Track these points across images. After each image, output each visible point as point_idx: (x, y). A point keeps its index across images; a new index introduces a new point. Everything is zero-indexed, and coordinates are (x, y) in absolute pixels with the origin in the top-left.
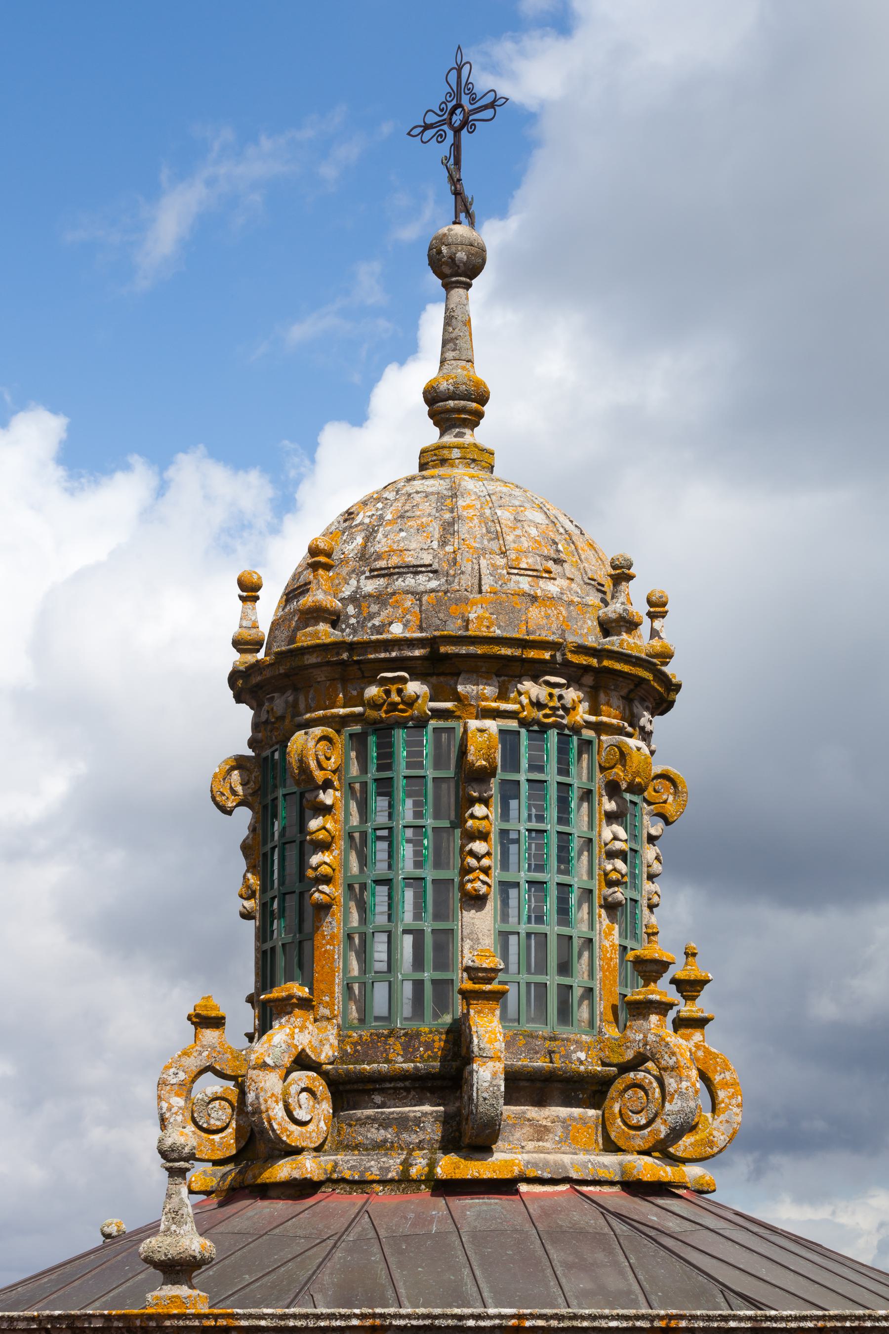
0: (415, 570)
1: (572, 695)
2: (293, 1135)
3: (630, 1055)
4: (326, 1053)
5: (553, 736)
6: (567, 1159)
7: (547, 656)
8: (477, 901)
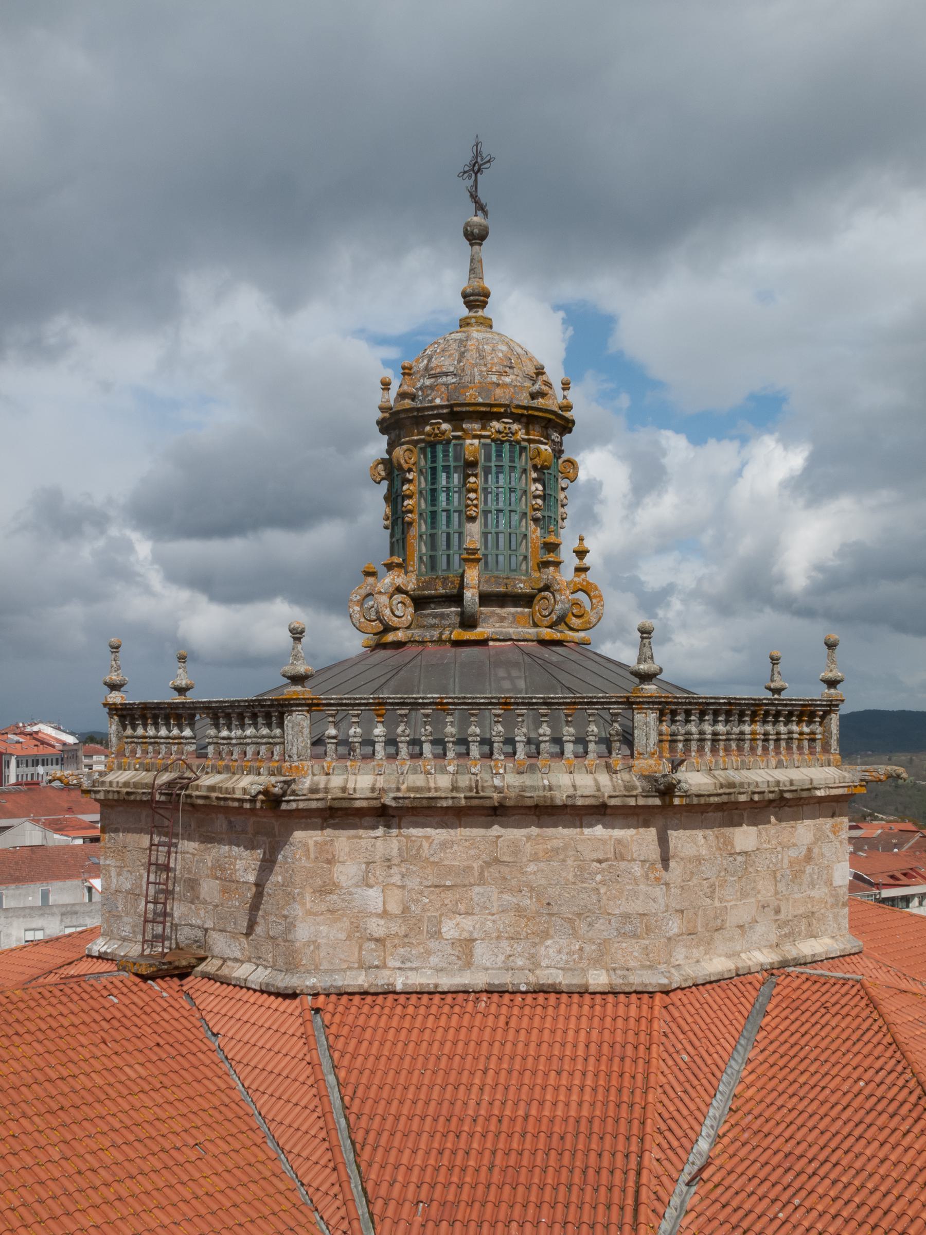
0: (446, 374)
1: (515, 427)
2: (395, 622)
3: (542, 585)
4: (410, 587)
5: (506, 446)
6: (511, 630)
7: (502, 410)
8: (472, 519)
